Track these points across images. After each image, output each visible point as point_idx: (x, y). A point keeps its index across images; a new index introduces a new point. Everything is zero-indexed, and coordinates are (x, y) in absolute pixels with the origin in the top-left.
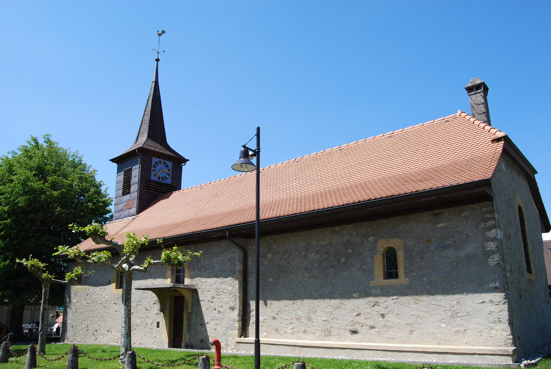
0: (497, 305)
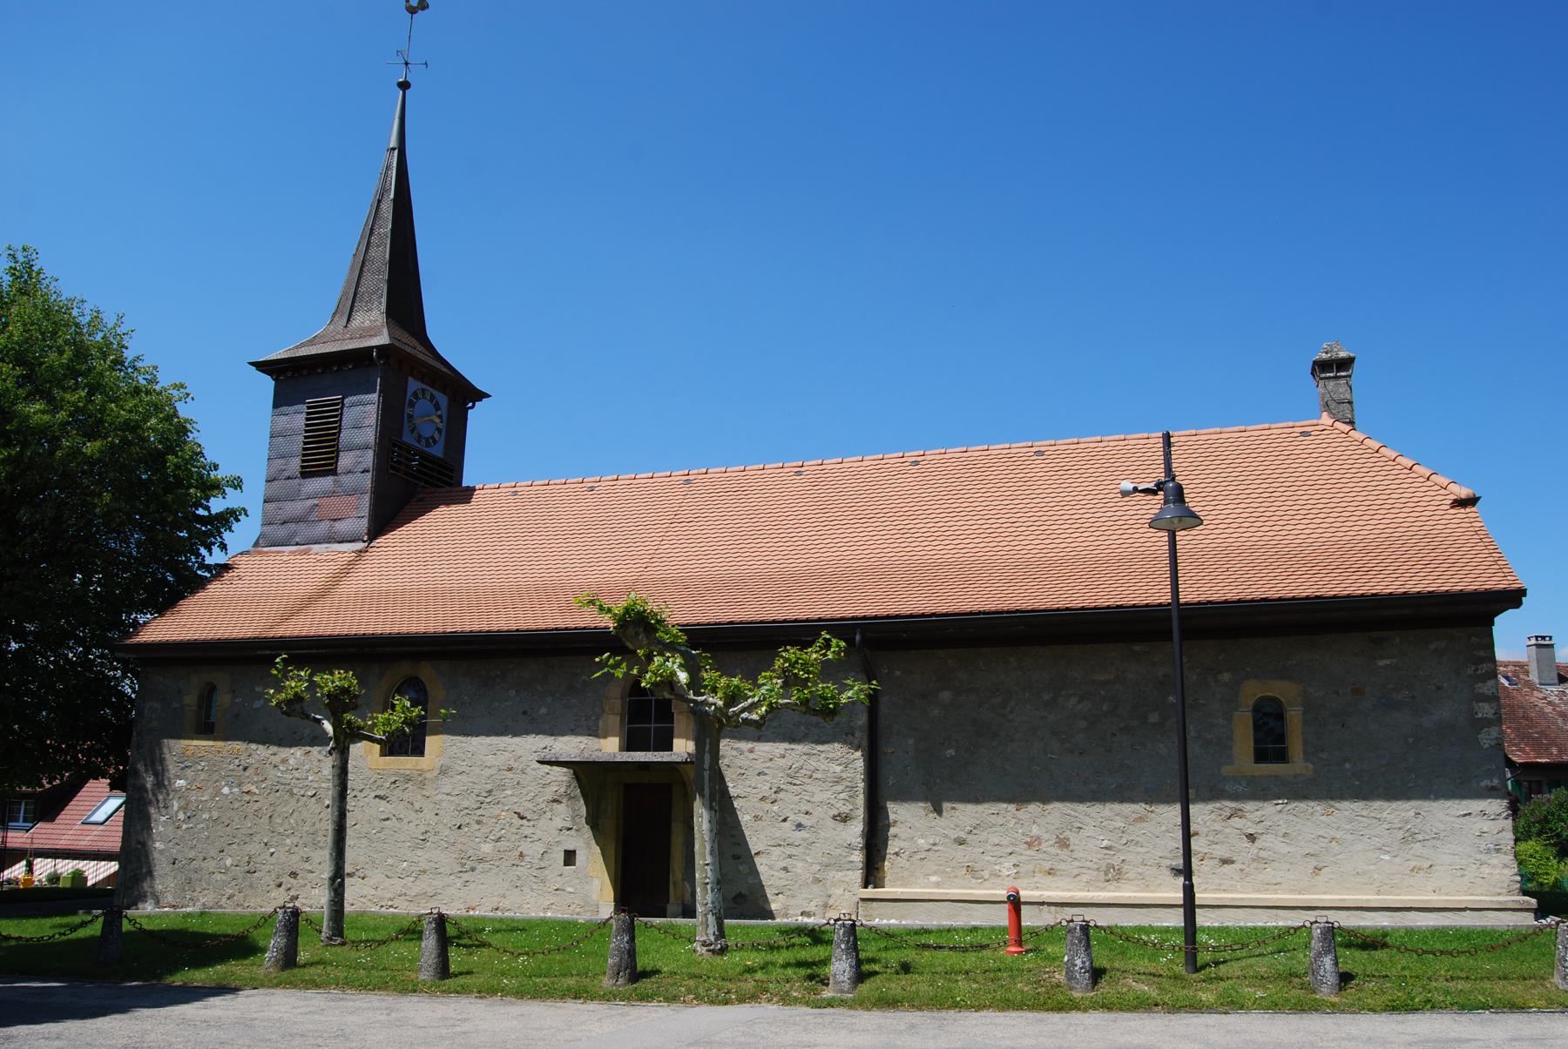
0: (1493, 819)
